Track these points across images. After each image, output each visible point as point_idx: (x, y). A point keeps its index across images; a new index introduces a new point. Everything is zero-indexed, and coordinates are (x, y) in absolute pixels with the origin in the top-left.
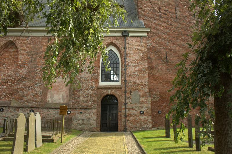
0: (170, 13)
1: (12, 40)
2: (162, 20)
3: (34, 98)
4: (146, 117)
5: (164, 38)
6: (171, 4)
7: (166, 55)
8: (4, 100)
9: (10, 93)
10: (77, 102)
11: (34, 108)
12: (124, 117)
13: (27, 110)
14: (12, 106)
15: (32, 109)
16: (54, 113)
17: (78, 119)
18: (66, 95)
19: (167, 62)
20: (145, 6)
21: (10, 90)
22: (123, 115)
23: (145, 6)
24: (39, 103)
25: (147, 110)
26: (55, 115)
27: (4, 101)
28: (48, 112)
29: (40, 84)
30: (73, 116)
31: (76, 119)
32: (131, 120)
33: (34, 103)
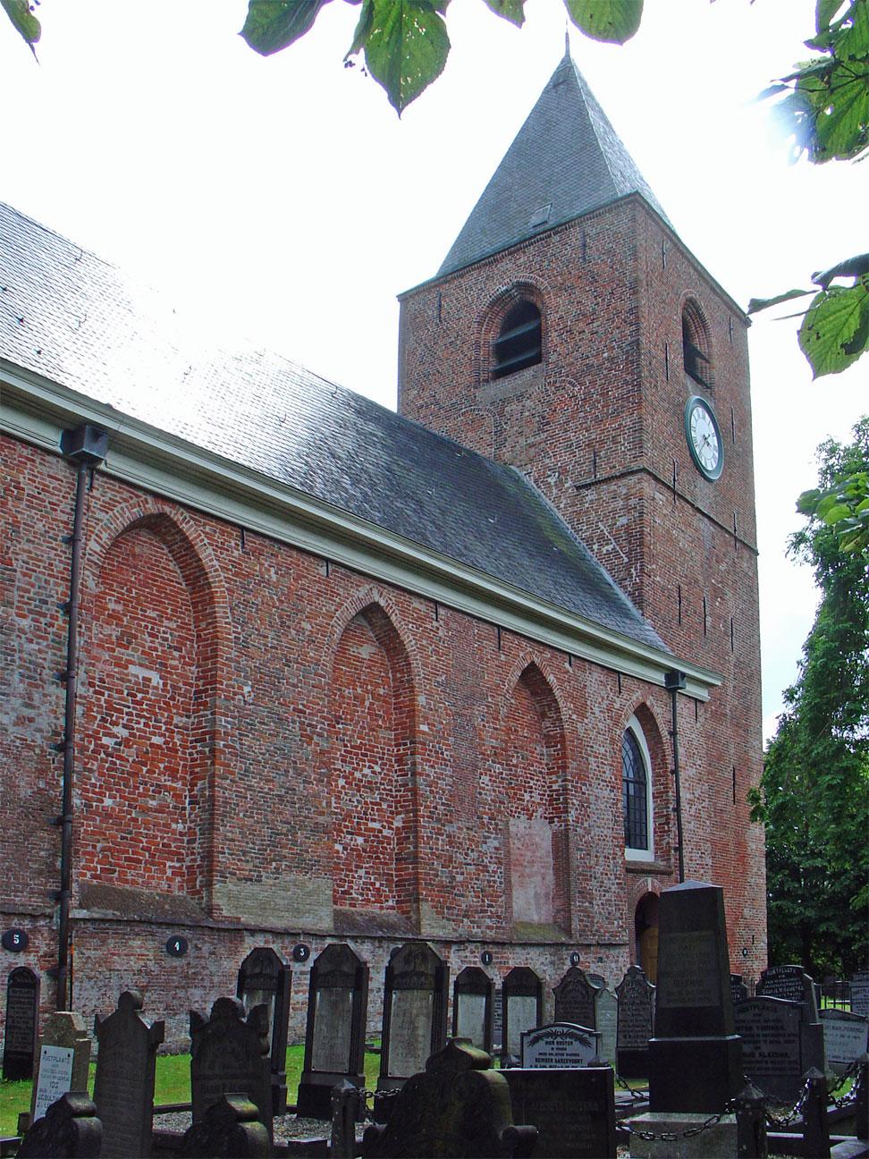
8: (362, 906)
9: (379, 874)
18: (543, 892)
21: (378, 858)
29: (496, 844)
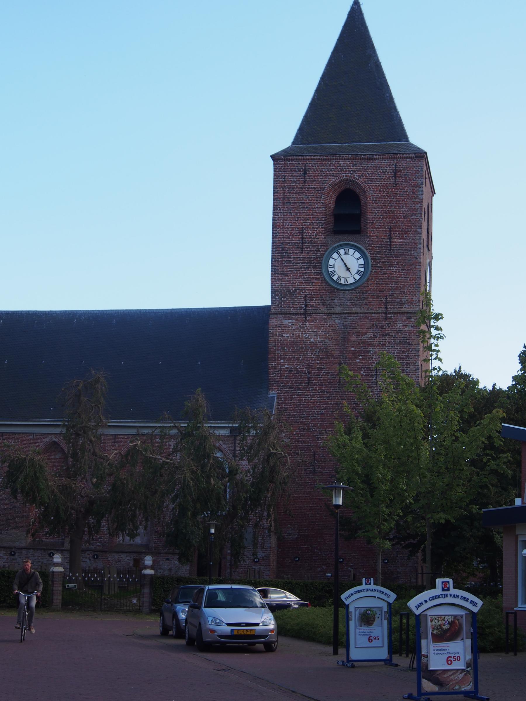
0: (328, 373)
1: (57, 440)
2: (311, 389)
3: (98, 537)
4: (262, 567)
5: (314, 426)
6: (332, 355)
7: (314, 458)
10: (161, 544)
11: (99, 553)
12: (230, 566)
13: (88, 554)
14: (65, 549)
15: (96, 553)
16: (128, 560)
17: (163, 569)
19: (314, 471)
20: (282, 361)
22: (228, 564)
23: (282, 361)
24: (106, 544)
25: (265, 556)
26: (129, 563)
27: (52, 540)
28: (119, 558)
30: (156, 565)
31: (160, 569)
32: (240, 571)
33: (99, 544)
